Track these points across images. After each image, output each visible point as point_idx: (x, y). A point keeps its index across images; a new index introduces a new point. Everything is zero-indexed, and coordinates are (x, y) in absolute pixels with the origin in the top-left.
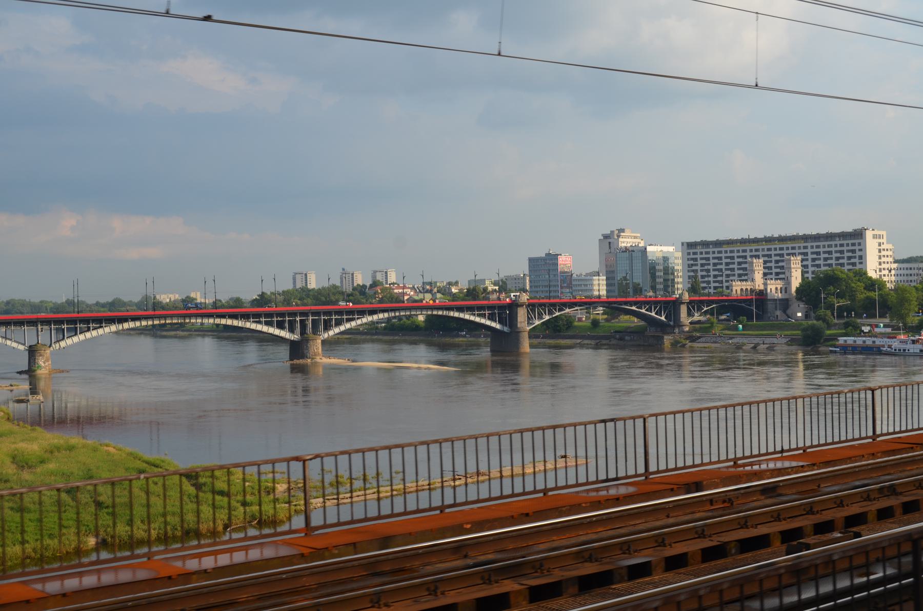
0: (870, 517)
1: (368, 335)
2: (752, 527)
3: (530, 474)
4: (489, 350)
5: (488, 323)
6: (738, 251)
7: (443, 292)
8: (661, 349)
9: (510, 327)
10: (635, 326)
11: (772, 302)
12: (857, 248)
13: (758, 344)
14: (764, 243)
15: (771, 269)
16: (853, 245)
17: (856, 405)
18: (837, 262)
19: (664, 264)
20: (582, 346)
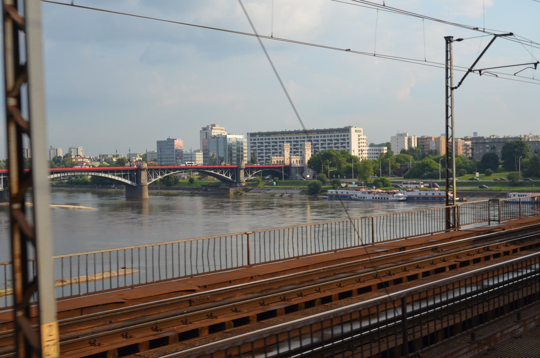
0: (404, 280)
1: (56, 187)
2: (363, 282)
3: (122, 275)
4: (125, 196)
5: (123, 180)
6: (280, 139)
7: (107, 161)
8: (228, 197)
9: (137, 183)
10: (214, 182)
11: (294, 169)
12: (346, 137)
13: (283, 194)
14: (294, 134)
15: (277, 150)
16: (344, 136)
17: (325, 233)
18: (335, 146)
19: (237, 145)
20: (183, 195)
